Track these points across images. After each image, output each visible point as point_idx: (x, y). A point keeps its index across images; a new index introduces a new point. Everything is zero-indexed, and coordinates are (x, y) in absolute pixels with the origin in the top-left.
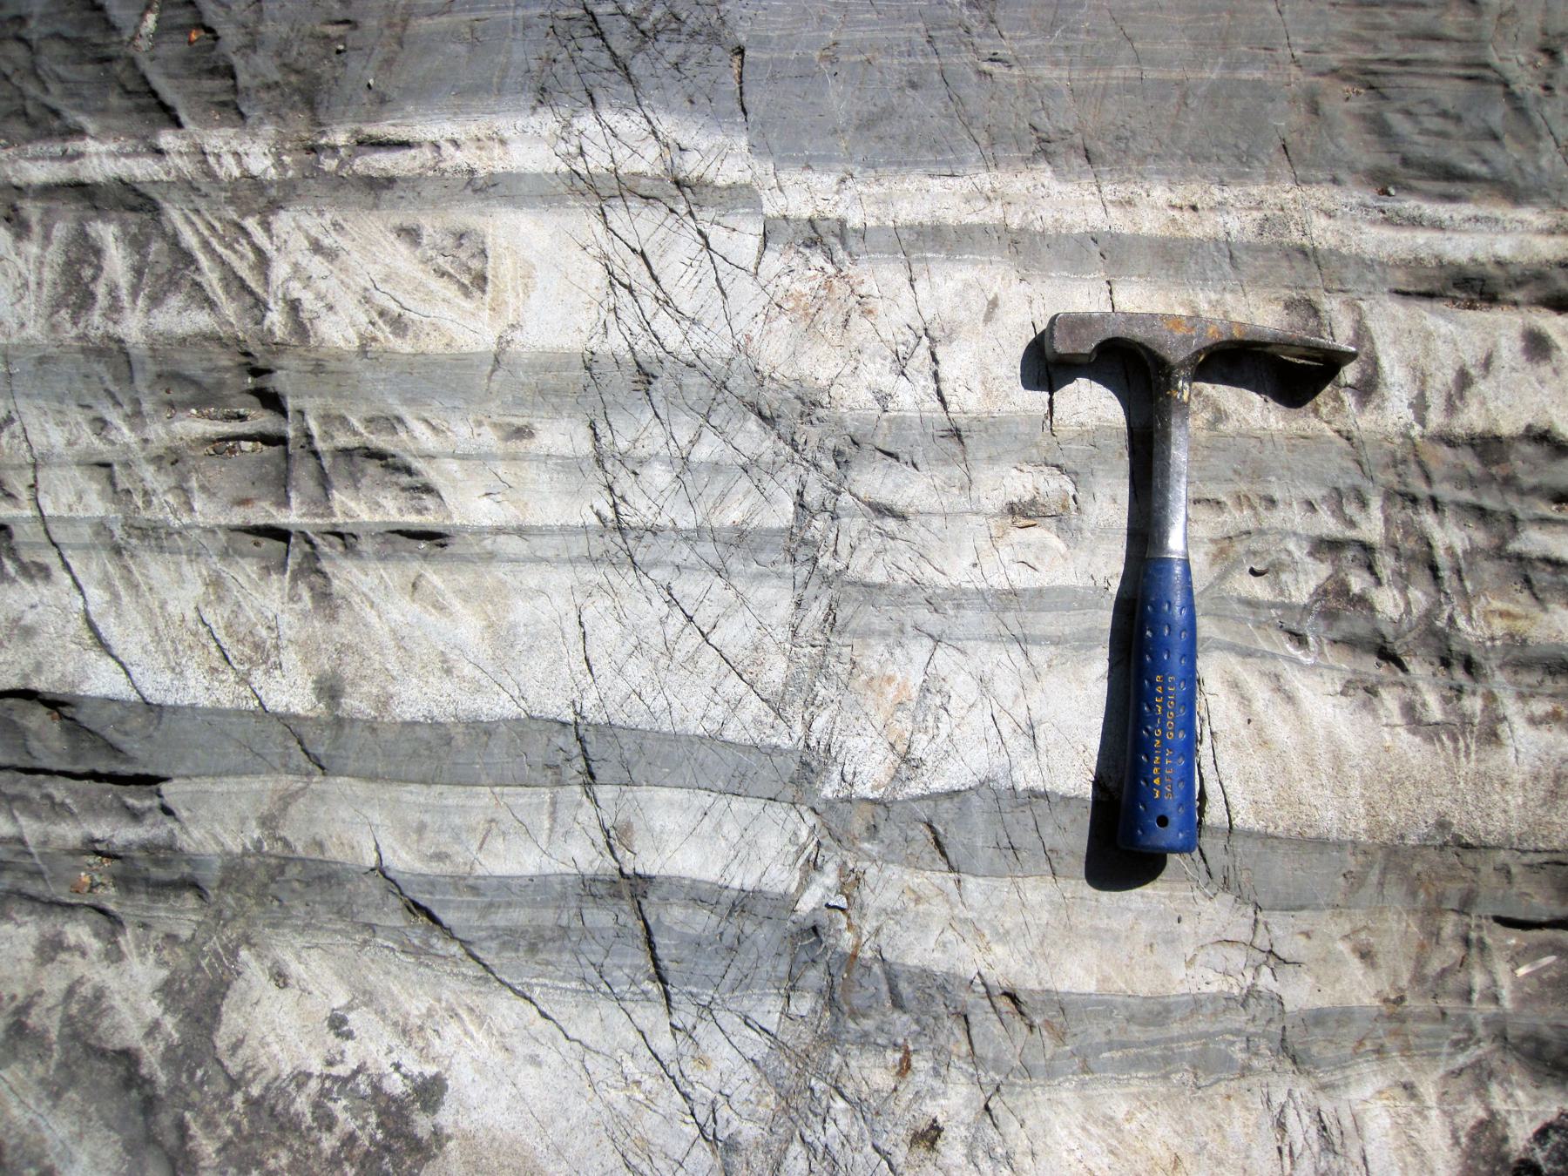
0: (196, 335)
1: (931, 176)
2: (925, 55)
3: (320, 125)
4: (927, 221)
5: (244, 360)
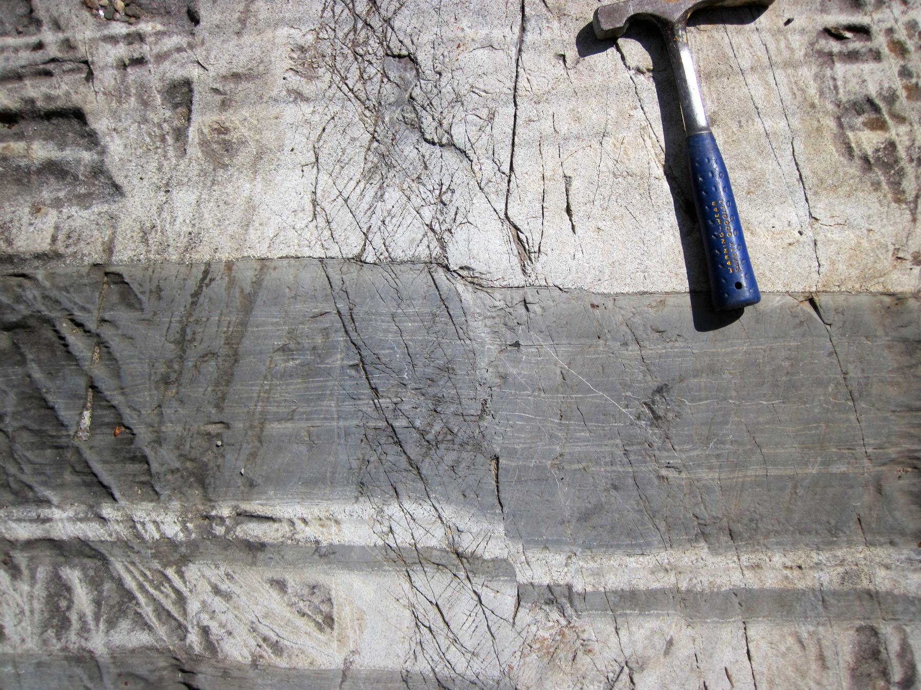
0: (141, 647)
1: (629, 555)
2: (623, 465)
3: (210, 500)
4: (626, 588)
5: (175, 662)
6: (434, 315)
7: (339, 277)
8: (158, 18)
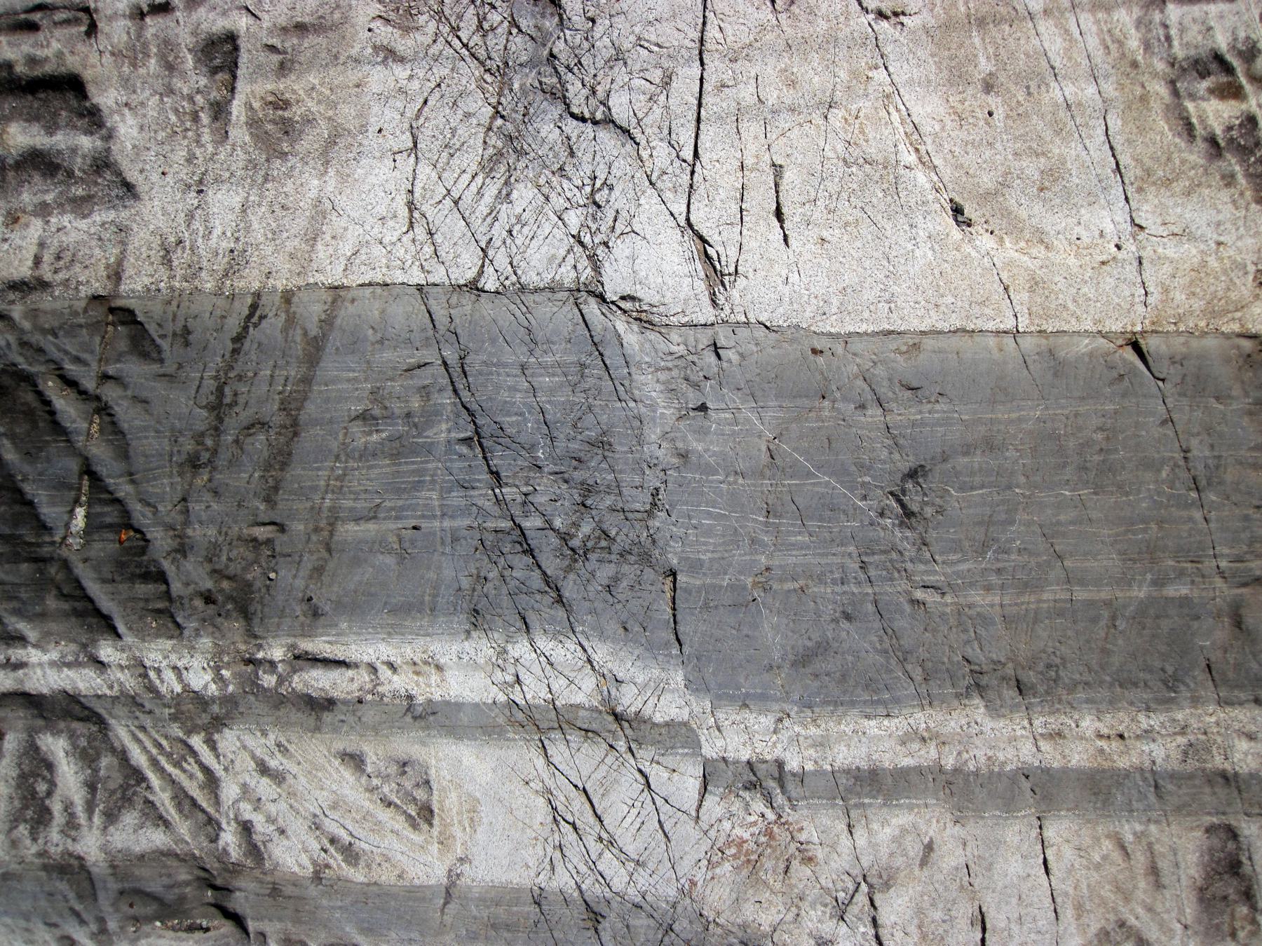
0: (154, 852)
1: (868, 717)
3: (256, 637)
4: (864, 765)
6: (583, 365)
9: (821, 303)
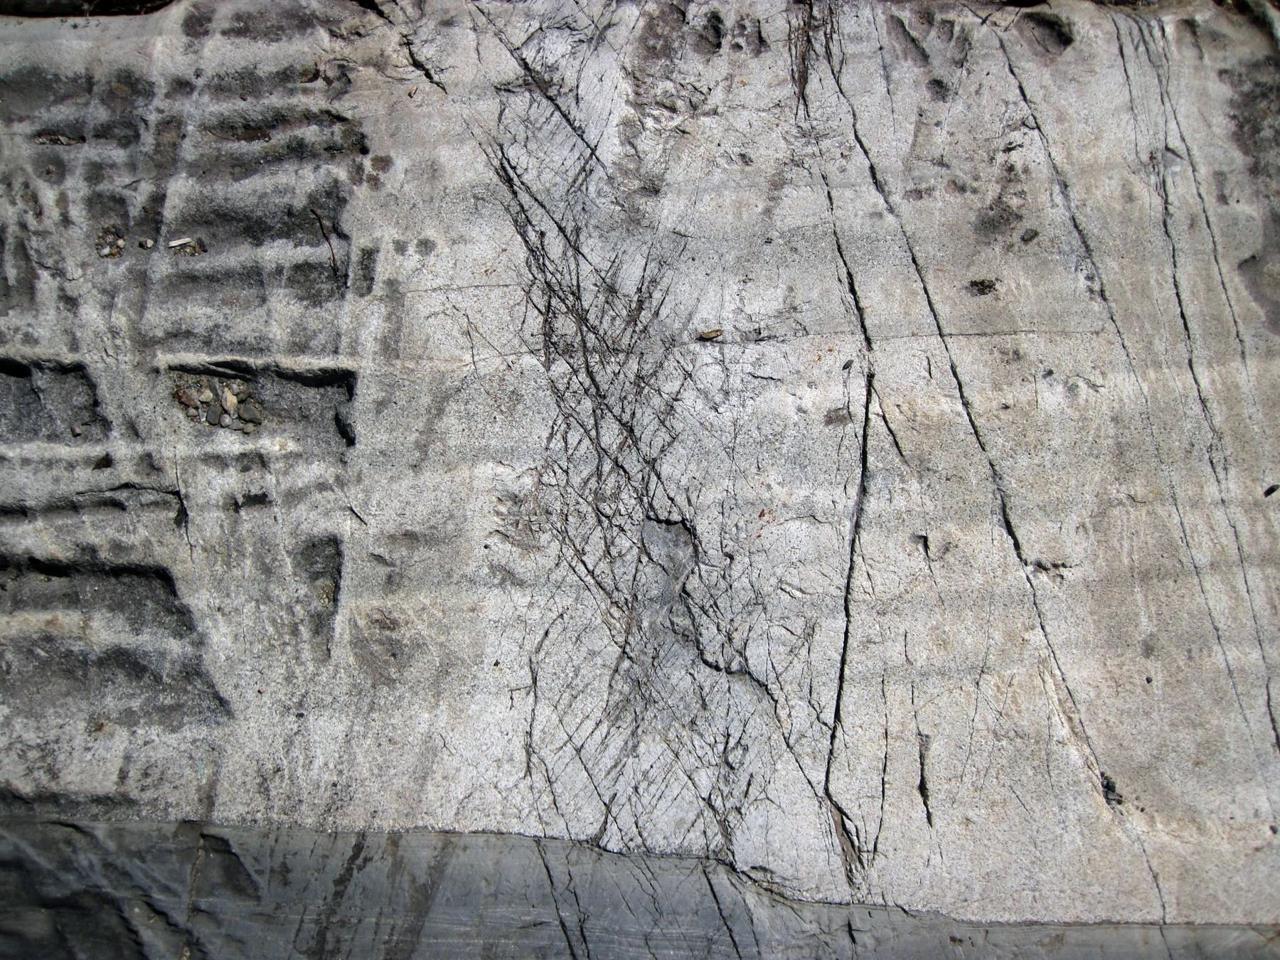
6: (711, 941)
7: (563, 869)
8: (289, 425)
9: (963, 888)
